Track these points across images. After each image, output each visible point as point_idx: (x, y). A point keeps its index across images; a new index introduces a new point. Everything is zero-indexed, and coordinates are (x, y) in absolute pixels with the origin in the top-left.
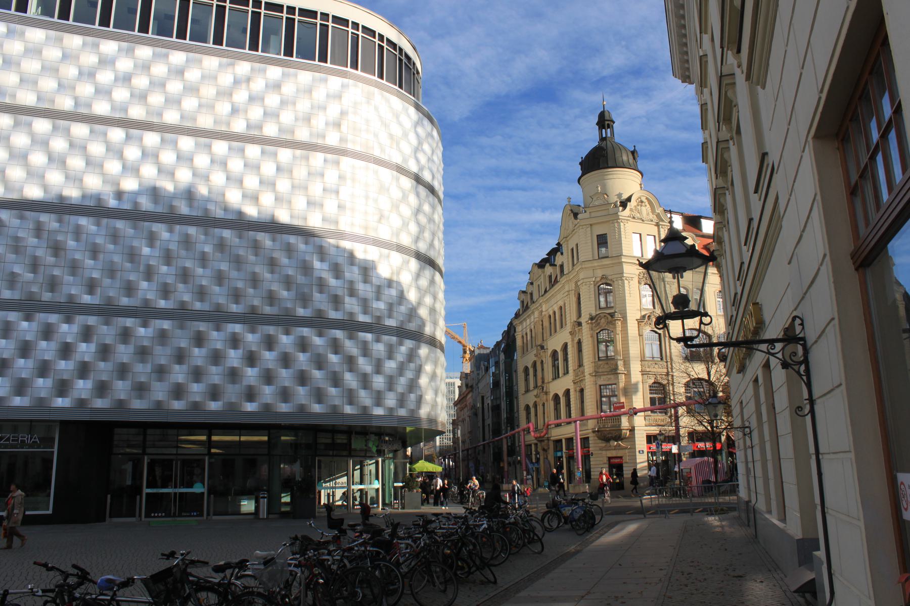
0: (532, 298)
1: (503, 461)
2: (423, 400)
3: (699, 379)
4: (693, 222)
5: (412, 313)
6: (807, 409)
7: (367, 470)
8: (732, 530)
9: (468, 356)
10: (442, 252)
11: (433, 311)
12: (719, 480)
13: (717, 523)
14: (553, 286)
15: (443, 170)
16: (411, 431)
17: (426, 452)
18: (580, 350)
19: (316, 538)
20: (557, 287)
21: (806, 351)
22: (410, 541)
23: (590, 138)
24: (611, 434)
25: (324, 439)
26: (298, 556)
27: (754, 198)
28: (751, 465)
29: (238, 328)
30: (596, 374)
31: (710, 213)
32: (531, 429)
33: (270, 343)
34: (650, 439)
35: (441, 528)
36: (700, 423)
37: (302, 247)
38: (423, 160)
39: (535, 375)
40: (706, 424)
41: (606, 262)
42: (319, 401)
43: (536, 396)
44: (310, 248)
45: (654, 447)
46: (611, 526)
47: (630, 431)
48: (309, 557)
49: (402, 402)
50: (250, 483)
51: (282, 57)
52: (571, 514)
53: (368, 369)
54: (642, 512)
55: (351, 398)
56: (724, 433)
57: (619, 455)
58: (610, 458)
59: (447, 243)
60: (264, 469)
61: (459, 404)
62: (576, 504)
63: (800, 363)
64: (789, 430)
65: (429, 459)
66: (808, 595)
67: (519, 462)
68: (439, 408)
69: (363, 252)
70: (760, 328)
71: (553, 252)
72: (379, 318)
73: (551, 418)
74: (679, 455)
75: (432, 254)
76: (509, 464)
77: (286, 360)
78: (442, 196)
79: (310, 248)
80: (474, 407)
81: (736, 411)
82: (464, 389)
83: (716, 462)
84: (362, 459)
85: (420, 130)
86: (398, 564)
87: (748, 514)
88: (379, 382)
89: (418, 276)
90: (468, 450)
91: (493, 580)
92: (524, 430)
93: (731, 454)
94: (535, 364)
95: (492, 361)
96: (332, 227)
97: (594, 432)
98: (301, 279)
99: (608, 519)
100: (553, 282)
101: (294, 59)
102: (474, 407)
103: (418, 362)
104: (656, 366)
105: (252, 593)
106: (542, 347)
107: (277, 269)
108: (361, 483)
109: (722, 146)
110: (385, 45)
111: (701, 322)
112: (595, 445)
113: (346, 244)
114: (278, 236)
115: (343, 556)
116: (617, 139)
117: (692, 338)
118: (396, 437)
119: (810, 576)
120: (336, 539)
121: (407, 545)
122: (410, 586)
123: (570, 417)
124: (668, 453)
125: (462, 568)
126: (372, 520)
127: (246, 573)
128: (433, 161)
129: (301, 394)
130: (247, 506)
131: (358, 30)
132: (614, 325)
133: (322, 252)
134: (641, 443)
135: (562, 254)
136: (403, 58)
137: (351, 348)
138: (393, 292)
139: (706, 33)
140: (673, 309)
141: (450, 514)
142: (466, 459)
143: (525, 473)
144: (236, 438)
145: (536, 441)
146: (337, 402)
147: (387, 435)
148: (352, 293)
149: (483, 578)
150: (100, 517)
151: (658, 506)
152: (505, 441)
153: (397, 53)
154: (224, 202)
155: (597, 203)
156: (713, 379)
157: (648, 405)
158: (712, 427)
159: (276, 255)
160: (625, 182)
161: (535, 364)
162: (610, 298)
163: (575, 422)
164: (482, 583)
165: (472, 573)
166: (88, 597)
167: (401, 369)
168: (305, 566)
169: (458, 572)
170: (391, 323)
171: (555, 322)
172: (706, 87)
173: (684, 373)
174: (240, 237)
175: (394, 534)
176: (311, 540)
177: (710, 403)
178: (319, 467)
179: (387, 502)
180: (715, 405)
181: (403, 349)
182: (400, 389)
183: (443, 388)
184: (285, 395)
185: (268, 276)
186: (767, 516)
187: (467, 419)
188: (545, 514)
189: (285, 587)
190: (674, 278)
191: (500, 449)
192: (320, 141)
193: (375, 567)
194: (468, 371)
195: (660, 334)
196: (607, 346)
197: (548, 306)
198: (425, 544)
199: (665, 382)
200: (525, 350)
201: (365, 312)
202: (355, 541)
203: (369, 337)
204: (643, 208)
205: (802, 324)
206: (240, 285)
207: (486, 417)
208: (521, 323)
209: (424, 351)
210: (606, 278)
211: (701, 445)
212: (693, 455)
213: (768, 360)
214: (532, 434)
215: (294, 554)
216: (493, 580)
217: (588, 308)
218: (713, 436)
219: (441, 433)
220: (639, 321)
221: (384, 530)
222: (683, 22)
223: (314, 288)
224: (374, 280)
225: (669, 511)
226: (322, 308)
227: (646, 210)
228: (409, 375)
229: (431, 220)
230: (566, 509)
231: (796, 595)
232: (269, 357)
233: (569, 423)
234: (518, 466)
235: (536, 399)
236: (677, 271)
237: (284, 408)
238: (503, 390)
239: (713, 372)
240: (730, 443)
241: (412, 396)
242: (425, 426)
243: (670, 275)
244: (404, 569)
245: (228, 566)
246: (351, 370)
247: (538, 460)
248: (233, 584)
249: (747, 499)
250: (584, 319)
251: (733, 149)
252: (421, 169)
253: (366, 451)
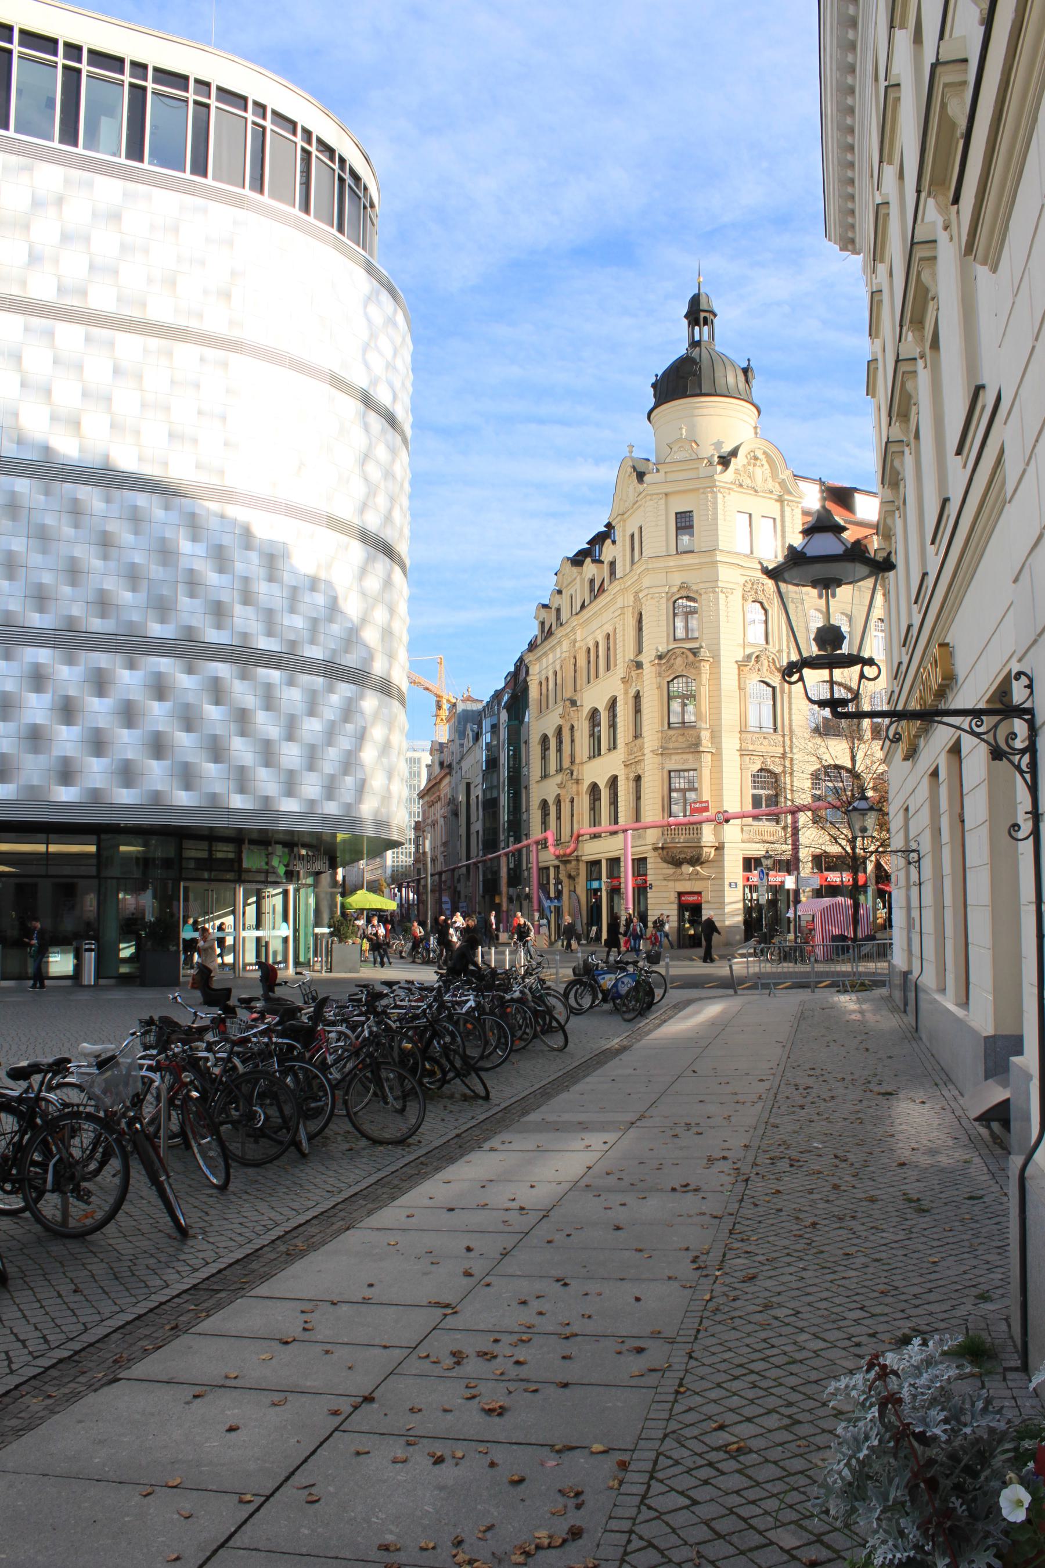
0: (558, 618)
1: (500, 894)
2: (367, 788)
3: (837, 767)
4: (842, 497)
5: (351, 638)
6: (1026, 827)
7: (267, 904)
8: (878, 1018)
9: (445, 713)
10: (407, 532)
11: (387, 633)
12: (860, 935)
13: (853, 1006)
14: (596, 597)
15: (413, 385)
16: (344, 841)
17: (368, 877)
18: (638, 711)
19: (184, 1019)
20: (603, 599)
21: (1033, 731)
22: (343, 1028)
23: (673, 341)
24: (684, 855)
25: (195, 851)
26: (154, 1052)
27: (954, 463)
28: (915, 914)
29: (43, 655)
30: (664, 752)
31: (875, 486)
32: (550, 842)
33: (100, 683)
34: (749, 864)
35: (396, 1007)
36: (835, 840)
37: (159, 513)
38: (378, 366)
39: (559, 750)
40: (844, 843)
41: (688, 559)
42: (188, 786)
43: (560, 786)
44: (173, 517)
45: (754, 876)
46: (680, 1006)
47: (717, 849)
48: (175, 1055)
49: (330, 791)
50: (68, 925)
51: (122, 160)
52: (615, 985)
53: (274, 732)
54: (731, 984)
55: (242, 780)
56: (873, 858)
57: (695, 890)
58: (680, 894)
59: (415, 516)
60: (90, 903)
61: (429, 793)
62: (624, 970)
63: (1023, 752)
64: (986, 857)
65: (374, 888)
66: (995, 1126)
67: (528, 897)
68: (395, 801)
69: (267, 528)
70: (947, 686)
71: (599, 539)
72: (293, 644)
73: (585, 827)
74: (797, 892)
75: (389, 535)
76: (510, 900)
77: (129, 714)
78: (409, 432)
79: (173, 517)
80: (452, 801)
81: (896, 822)
82: (437, 769)
83: (856, 906)
84: (259, 886)
85: (373, 310)
86: (324, 1067)
87: (906, 993)
88: (291, 754)
89: (363, 572)
90: (440, 874)
91: (483, 1093)
92: (537, 843)
93: (882, 895)
94: (560, 730)
95: (486, 724)
96: (214, 480)
97: (655, 849)
98: (156, 571)
99: (675, 995)
100: (596, 590)
101: (146, 165)
102: (452, 801)
103: (361, 723)
104: (766, 742)
105: (77, 1115)
106: (573, 703)
107: (114, 552)
108: (258, 926)
109: (903, 367)
110: (313, 149)
111: (862, 676)
112: (656, 871)
113: (234, 511)
114: (117, 493)
115: (231, 1053)
116: (719, 346)
117: (844, 702)
118: (319, 850)
119: (998, 1094)
120: (218, 1023)
121: (340, 1033)
122: (345, 1102)
123: (616, 822)
124: (777, 889)
125: (431, 1074)
126: (279, 992)
127: (67, 1080)
128: (394, 368)
129: (156, 774)
130: (60, 963)
131: (264, 118)
132: (698, 668)
133: (194, 525)
134: (733, 869)
135: (614, 542)
136: (347, 176)
137: (243, 693)
138: (320, 599)
139: (890, 163)
140: (815, 650)
141: (412, 982)
142: (438, 889)
143: (537, 915)
144: (41, 848)
145: (556, 863)
146: (218, 788)
147: (304, 846)
148: (247, 598)
149: (468, 1092)
151: (759, 976)
152: (503, 861)
153: (336, 167)
154: (17, 428)
155: (678, 456)
156: (860, 767)
157: (748, 807)
158: (853, 848)
159: (112, 527)
160: (723, 421)
161: (560, 730)
162: (693, 623)
163: (625, 831)
164: (465, 1098)
165: (449, 1082)
167: (330, 734)
168: (167, 1069)
169: (425, 1080)
170: (314, 652)
171: (597, 660)
172: (882, 261)
173: (811, 756)
174: (47, 493)
175: (318, 1016)
176: (176, 1024)
177: (855, 809)
178: (186, 899)
179: (302, 959)
180: (863, 812)
181: (335, 699)
182: (328, 768)
183: (403, 768)
184: (127, 774)
185: (97, 564)
186: (938, 997)
187: (441, 821)
188: (571, 984)
189: (134, 1105)
190: (820, 596)
191: (496, 873)
192: (193, 324)
193: (285, 1073)
194: (444, 739)
195: (774, 688)
196: (684, 705)
197: (584, 632)
198: (371, 1033)
199: (778, 769)
200: (543, 707)
201: (270, 633)
202: (252, 1026)
203: (275, 675)
204: (758, 471)
205: (1030, 686)
206: (47, 578)
207: (473, 818)
208: (539, 659)
209: (370, 702)
210: (688, 588)
211: (834, 877)
212: (818, 893)
213: (958, 742)
214: (552, 849)
215: (146, 1048)
216: (483, 1093)
217: (656, 640)
218: (853, 863)
219: (394, 844)
220: (741, 665)
221: (300, 1009)
222: (849, 140)
223: (181, 588)
224: (286, 577)
225: (776, 984)
226: (194, 623)
227: (761, 472)
228: (345, 743)
229: (388, 474)
230: (607, 977)
231: (976, 1124)
232: (99, 709)
233: (615, 833)
234: (525, 903)
235: (559, 791)
236: (827, 584)
237: (125, 796)
238: (504, 773)
239: (860, 756)
240: (882, 876)
241: (349, 780)
242: (369, 831)
243: (814, 592)
244: (335, 1075)
245: (35, 1068)
246: (243, 734)
247: (559, 894)
248: (44, 1099)
249: (905, 968)
251: (924, 376)
252: (375, 382)
253: (267, 872)
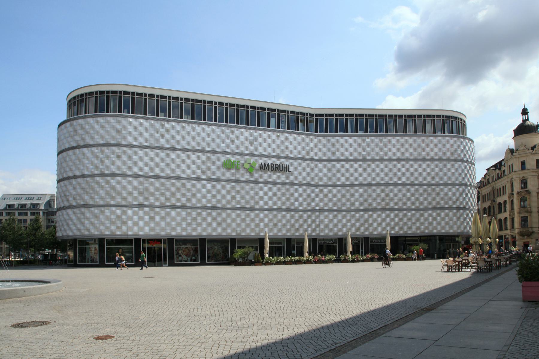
23: (519, 121)
30: (519, 213)
100: (499, 177)
106: (494, 201)
166: (464, 261)
250: (515, 192)
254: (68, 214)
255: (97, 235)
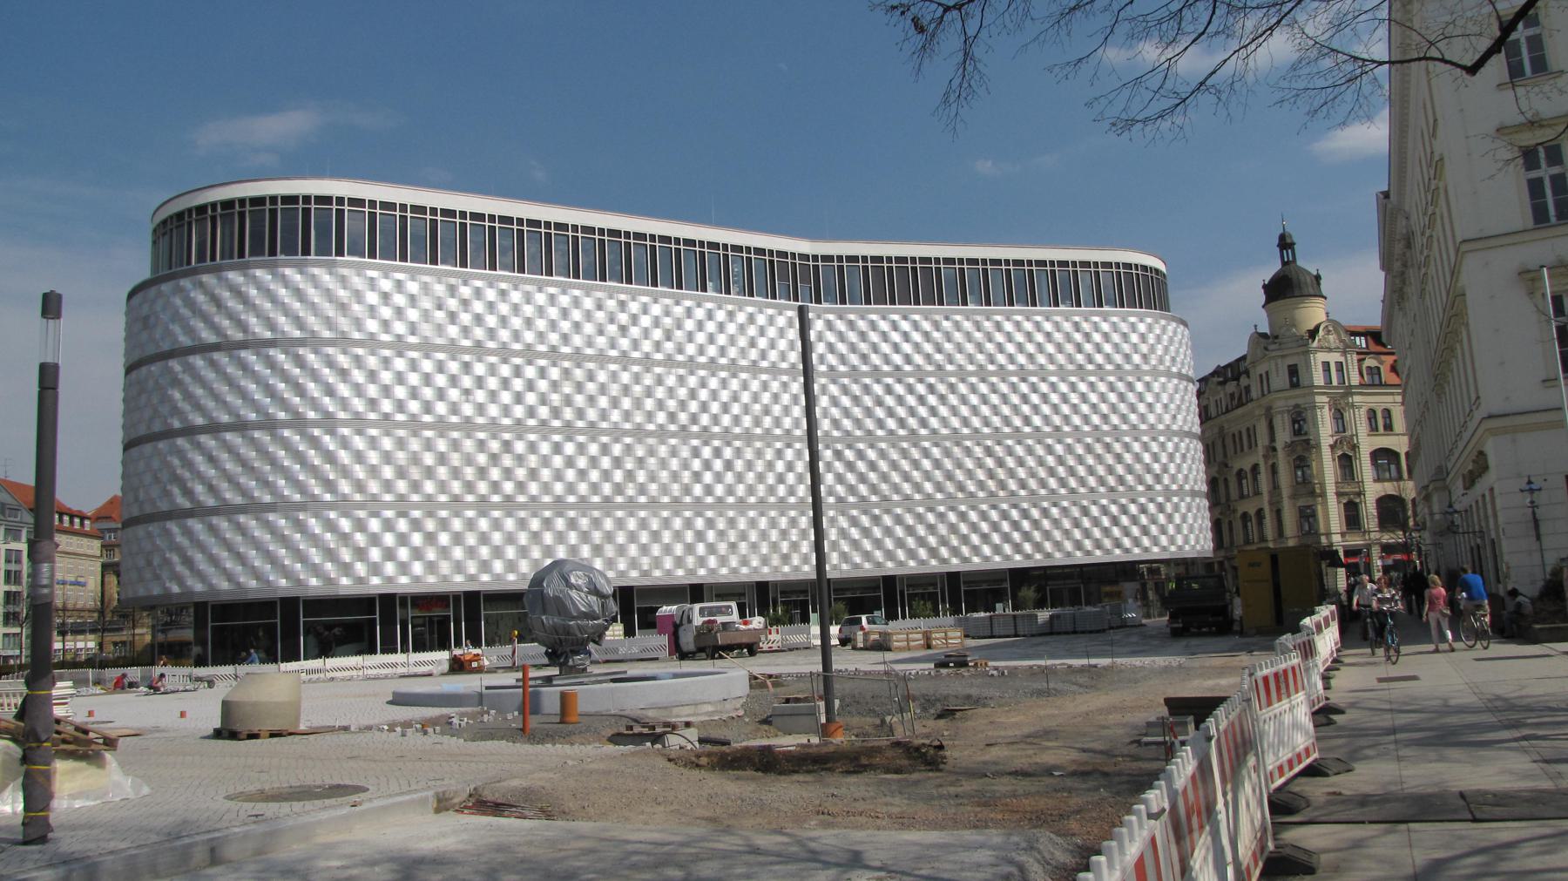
23: (1272, 268)
30: (1294, 496)
41: (1297, 392)
150: (282, 599)
250: (1279, 445)
254: (188, 533)
255: (226, 592)
